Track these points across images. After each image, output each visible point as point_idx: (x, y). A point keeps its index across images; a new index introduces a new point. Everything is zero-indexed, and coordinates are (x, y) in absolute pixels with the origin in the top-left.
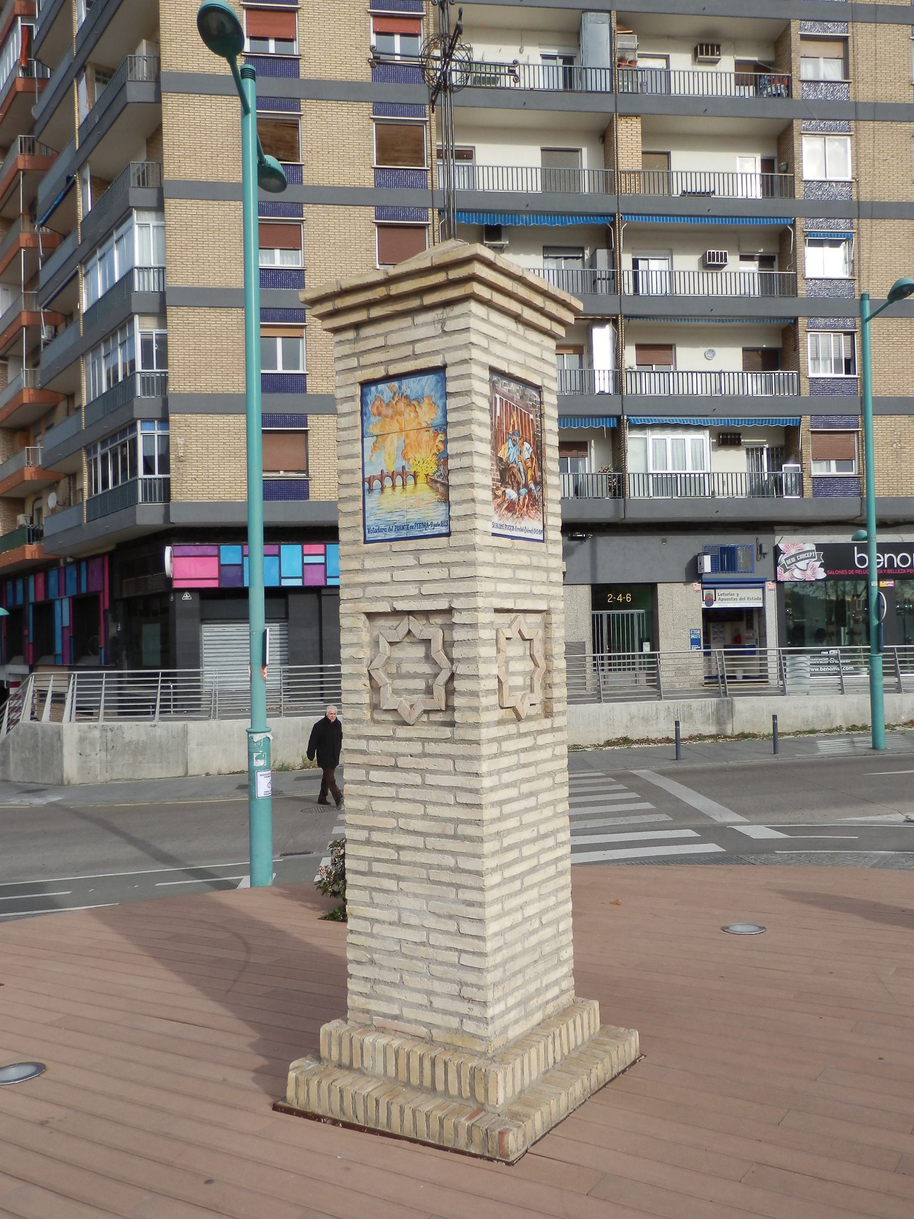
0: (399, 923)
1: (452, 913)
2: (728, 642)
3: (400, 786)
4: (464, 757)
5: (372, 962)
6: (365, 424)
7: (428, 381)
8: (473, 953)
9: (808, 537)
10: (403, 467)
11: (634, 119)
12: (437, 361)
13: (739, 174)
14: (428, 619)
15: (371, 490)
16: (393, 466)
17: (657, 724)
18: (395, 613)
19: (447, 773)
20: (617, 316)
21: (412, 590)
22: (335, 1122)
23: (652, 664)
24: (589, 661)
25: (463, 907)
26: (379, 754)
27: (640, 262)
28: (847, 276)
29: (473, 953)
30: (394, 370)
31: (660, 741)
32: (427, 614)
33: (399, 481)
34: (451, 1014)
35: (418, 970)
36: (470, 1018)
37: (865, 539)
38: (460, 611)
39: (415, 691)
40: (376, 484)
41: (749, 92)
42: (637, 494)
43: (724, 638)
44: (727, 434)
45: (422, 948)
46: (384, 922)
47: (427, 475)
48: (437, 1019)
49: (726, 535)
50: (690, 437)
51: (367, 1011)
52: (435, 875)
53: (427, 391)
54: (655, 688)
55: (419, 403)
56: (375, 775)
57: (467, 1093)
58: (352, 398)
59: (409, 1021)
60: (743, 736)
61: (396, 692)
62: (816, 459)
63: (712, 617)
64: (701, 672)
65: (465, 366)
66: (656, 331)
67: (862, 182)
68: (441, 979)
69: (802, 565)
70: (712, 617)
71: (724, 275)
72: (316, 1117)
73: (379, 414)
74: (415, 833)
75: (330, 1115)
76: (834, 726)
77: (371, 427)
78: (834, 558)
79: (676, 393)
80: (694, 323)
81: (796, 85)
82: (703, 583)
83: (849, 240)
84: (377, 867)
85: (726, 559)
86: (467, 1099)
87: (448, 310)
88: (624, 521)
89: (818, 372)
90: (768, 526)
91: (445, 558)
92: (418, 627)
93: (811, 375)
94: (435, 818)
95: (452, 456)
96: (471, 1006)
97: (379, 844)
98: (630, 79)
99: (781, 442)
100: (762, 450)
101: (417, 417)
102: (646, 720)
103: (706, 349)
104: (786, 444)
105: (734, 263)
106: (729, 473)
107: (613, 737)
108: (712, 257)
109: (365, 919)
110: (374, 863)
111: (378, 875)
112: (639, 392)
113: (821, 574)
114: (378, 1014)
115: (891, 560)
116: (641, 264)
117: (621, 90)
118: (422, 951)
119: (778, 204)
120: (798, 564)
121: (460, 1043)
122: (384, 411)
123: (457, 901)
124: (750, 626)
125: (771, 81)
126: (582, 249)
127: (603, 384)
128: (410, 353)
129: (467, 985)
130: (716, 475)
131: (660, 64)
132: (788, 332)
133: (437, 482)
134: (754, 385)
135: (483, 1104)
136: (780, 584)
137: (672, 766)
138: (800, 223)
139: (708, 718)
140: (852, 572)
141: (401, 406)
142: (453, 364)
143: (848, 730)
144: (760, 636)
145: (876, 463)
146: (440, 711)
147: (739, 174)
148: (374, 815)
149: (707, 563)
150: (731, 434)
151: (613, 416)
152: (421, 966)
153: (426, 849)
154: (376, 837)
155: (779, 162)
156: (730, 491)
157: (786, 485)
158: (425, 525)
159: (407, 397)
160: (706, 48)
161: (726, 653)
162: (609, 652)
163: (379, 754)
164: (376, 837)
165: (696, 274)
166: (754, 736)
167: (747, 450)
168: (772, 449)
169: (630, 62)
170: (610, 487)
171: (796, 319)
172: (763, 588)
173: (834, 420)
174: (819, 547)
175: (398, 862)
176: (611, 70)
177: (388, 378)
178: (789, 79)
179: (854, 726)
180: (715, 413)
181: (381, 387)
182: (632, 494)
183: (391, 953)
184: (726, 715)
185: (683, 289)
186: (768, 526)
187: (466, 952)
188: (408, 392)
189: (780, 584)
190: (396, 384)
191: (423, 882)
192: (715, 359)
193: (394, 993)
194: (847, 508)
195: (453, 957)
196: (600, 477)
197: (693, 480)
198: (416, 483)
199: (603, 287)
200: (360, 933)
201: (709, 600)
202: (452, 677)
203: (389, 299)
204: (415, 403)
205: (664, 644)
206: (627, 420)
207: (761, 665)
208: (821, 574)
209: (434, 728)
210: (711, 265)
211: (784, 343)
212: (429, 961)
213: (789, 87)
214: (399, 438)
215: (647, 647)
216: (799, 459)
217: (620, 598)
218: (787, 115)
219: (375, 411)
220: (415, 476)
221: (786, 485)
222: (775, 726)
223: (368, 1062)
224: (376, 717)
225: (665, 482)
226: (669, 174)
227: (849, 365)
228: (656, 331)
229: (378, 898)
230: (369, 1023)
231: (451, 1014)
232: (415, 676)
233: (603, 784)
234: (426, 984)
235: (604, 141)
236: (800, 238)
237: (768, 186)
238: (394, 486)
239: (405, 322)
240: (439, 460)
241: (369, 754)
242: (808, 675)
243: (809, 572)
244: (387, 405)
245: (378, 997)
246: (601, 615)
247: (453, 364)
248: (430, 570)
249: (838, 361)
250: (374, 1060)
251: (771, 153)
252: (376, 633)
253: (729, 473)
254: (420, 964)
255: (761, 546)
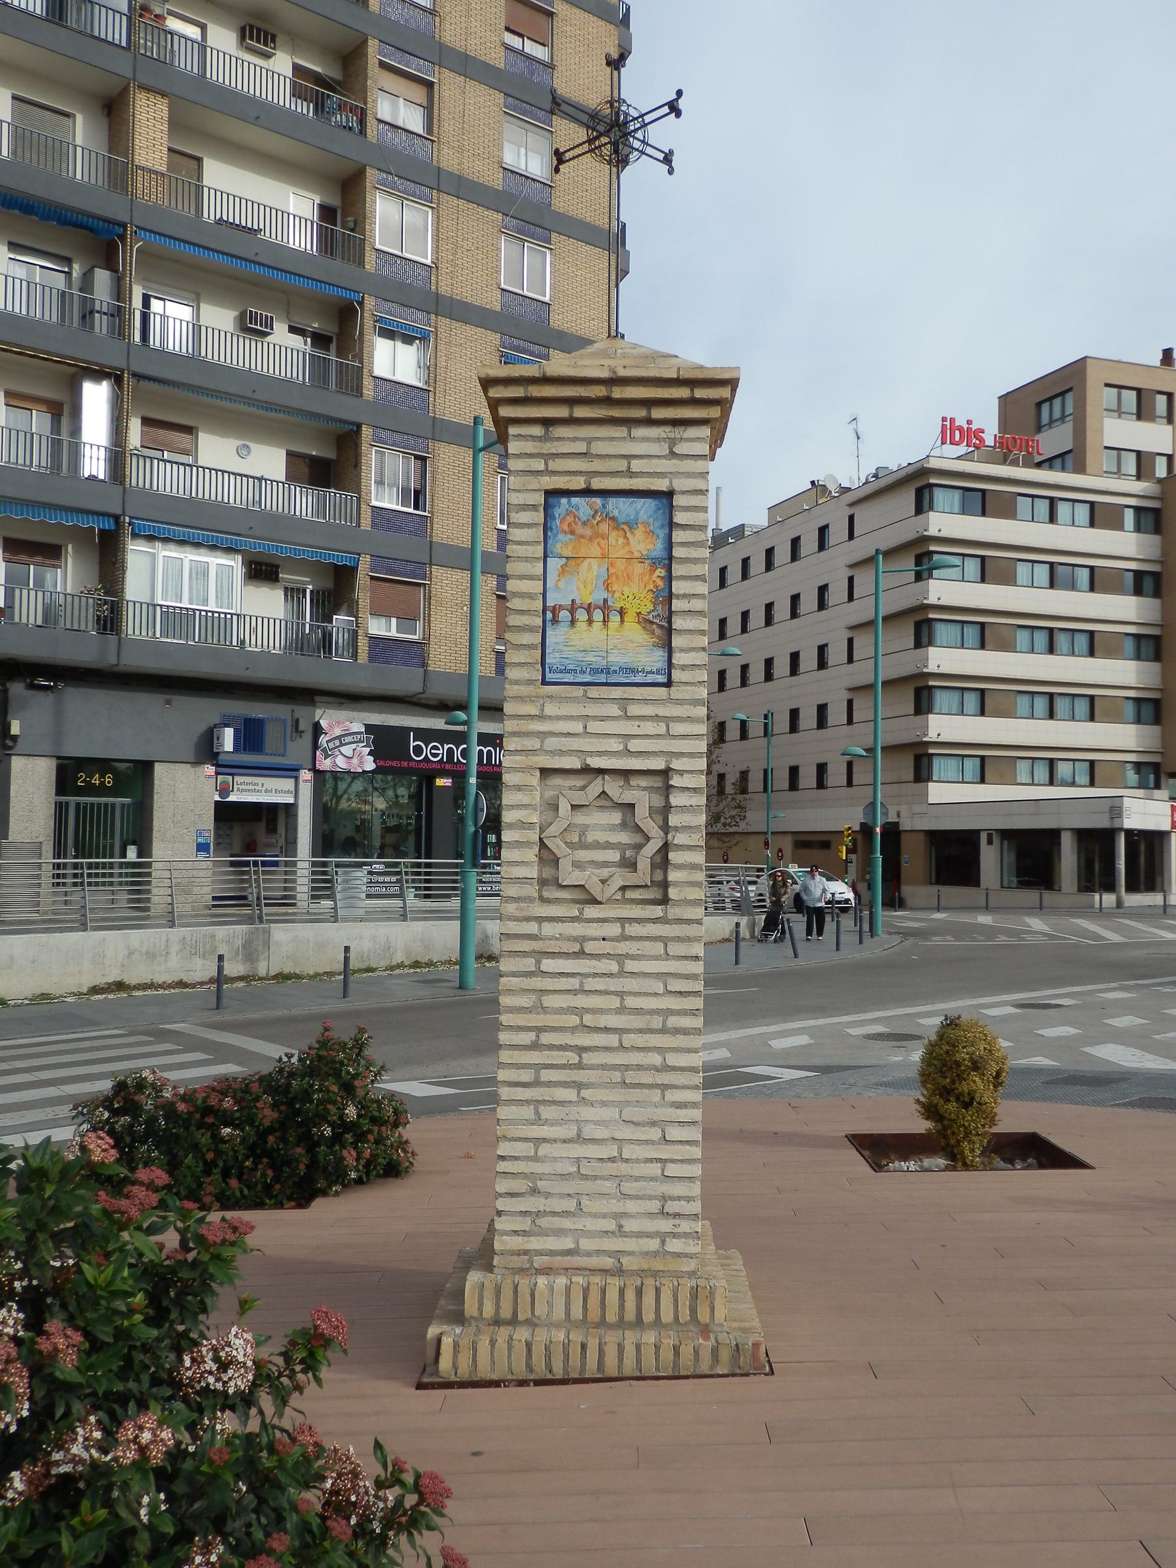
0: (579, 1139)
1: (656, 1118)
2: (237, 850)
3: (587, 975)
4: (678, 939)
5: (534, 1191)
6: (550, 541)
7: (645, 508)
8: (682, 1161)
9: (356, 714)
10: (605, 600)
11: (159, 97)
12: (662, 485)
13: (289, 213)
14: (627, 781)
15: (555, 621)
16: (587, 596)
17: (166, 961)
18: (586, 770)
19: (657, 958)
20: (122, 371)
21: (615, 745)
22: (522, 1383)
23: (139, 877)
24: (47, 871)
25: (672, 1110)
26: (557, 939)
27: (153, 301)
28: (420, 385)
29: (682, 1161)
30: (597, 484)
31: (170, 986)
32: (626, 774)
33: (598, 615)
34: (649, 1235)
35: (604, 1191)
36: (675, 1235)
37: (464, 723)
38: (681, 773)
39: (606, 864)
40: (564, 615)
41: (304, 108)
42: (137, 632)
43: (231, 844)
44: (261, 564)
45: (610, 1164)
46: (555, 1141)
47: (639, 614)
48: (630, 1244)
49: (255, 703)
50: (216, 561)
51: (526, 1252)
52: (631, 1077)
53: (643, 516)
54: (139, 909)
55: (631, 528)
56: (548, 965)
57: (685, 1315)
58: (534, 507)
59: (588, 1254)
60: (282, 977)
61: (577, 865)
62: (374, 614)
63: (227, 813)
64: (207, 889)
65: (700, 497)
66: (172, 400)
67: (442, 271)
68: (637, 1197)
69: (347, 750)
70: (227, 813)
71: (265, 345)
72: (496, 1384)
73: (572, 533)
74: (606, 1030)
75: (510, 1377)
76: (394, 963)
77: (559, 546)
78: (386, 743)
79: (200, 496)
80: (227, 404)
81: (371, 123)
82: (217, 766)
83: (424, 339)
84: (546, 1075)
85: (251, 736)
86: (686, 1324)
87: (681, 429)
88: (116, 669)
89: (382, 500)
90: (307, 695)
91: (663, 711)
92: (613, 788)
93: (374, 503)
94: (638, 1011)
95: (678, 597)
96: (677, 1222)
97: (552, 1047)
98: (156, 40)
99: (329, 584)
100: (304, 591)
101: (628, 544)
102: (150, 956)
103: (240, 443)
104: (335, 589)
105: (281, 334)
106: (262, 617)
107: (100, 981)
108: (253, 318)
109: (527, 1140)
110: (543, 1071)
111: (549, 1084)
112: (147, 486)
113: (370, 765)
114: (540, 1253)
115: (450, 751)
116: (156, 306)
117: (142, 51)
118: (611, 1168)
119: (337, 269)
120: (343, 749)
121: (661, 1268)
122: (579, 529)
123: (663, 1103)
124: (272, 829)
125: (341, 107)
126: (68, 261)
127: (94, 464)
128: (624, 469)
129: (672, 1198)
130: (248, 618)
131: (193, 32)
132: (347, 440)
133: (652, 623)
134: (303, 503)
135: (707, 1326)
136: (317, 773)
137: (217, 1017)
138: (370, 302)
139: (237, 953)
140: (405, 764)
141: (604, 527)
142: (683, 493)
143: (411, 967)
144: (286, 842)
145: (437, 627)
146: (646, 886)
147: (289, 213)
148: (545, 1013)
149: (228, 740)
150: (267, 565)
151: (109, 515)
152: (608, 1186)
153: (621, 1047)
154: (546, 1038)
155: (344, 216)
156: (265, 643)
157: (337, 643)
158: (634, 671)
159: (613, 519)
160: (258, 34)
161: (232, 864)
162: (76, 857)
163: (557, 939)
164: (546, 1038)
165: (229, 335)
166: (297, 976)
167: (286, 589)
168: (318, 592)
169: (156, 16)
170: (99, 617)
171: (359, 426)
172: (296, 778)
173: (396, 565)
174: (369, 729)
175: (580, 1066)
176: (129, 19)
177: (587, 492)
178: (363, 112)
179: (417, 962)
180: (251, 533)
181: (575, 500)
182: (130, 631)
183: (563, 1176)
184: (260, 948)
185: (212, 352)
186: (307, 695)
187: (672, 1161)
188: (616, 513)
189: (317, 773)
190: (598, 501)
191: (614, 1088)
192: (249, 458)
193: (567, 1223)
194: (404, 680)
195: (655, 1169)
196: (83, 599)
197: (203, 619)
198: (622, 621)
199: (101, 324)
200: (516, 1158)
201: (224, 791)
202: (665, 848)
203: (608, 401)
204: (625, 527)
205: (160, 850)
206: (130, 524)
207: (286, 881)
208: (370, 765)
209: (639, 906)
210: (252, 328)
211: (339, 455)
212: (619, 1178)
213: (362, 122)
214: (599, 566)
215: (132, 854)
216: (353, 611)
217: (96, 780)
218: (363, 159)
219: (566, 527)
220: (622, 612)
221: (337, 643)
222: (347, 959)
223: (541, 1309)
224: (546, 894)
225: (177, 619)
226: (199, 189)
227: (418, 497)
228: (172, 400)
229: (547, 1112)
230: (528, 1265)
231: (649, 1235)
232: (608, 846)
233: (138, 1044)
234: (615, 1206)
235: (109, 114)
236: (369, 323)
237: (327, 242)
238: (590, 621)
239: (621, 432)
240: (656, 597)
241: (541, 939)
242: (363, 896)
243: (355, 761)
244: (584, 523)
245: (544, 1233)
246: (67, 803)
247: (683, 493)
248: (642, 724)
249: (405, 491)
250: (550, 1304)
251: (334, 201)
252: (549, 793)
253: (262, 617)
254: (608, 1184)
255: (297, 721)
